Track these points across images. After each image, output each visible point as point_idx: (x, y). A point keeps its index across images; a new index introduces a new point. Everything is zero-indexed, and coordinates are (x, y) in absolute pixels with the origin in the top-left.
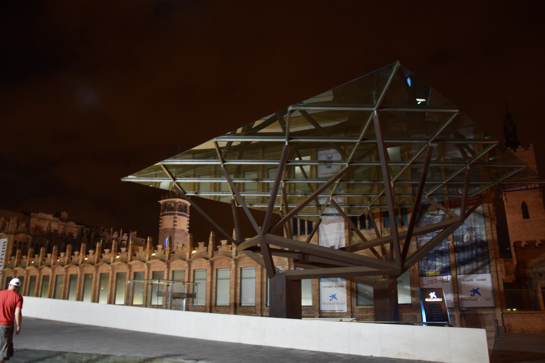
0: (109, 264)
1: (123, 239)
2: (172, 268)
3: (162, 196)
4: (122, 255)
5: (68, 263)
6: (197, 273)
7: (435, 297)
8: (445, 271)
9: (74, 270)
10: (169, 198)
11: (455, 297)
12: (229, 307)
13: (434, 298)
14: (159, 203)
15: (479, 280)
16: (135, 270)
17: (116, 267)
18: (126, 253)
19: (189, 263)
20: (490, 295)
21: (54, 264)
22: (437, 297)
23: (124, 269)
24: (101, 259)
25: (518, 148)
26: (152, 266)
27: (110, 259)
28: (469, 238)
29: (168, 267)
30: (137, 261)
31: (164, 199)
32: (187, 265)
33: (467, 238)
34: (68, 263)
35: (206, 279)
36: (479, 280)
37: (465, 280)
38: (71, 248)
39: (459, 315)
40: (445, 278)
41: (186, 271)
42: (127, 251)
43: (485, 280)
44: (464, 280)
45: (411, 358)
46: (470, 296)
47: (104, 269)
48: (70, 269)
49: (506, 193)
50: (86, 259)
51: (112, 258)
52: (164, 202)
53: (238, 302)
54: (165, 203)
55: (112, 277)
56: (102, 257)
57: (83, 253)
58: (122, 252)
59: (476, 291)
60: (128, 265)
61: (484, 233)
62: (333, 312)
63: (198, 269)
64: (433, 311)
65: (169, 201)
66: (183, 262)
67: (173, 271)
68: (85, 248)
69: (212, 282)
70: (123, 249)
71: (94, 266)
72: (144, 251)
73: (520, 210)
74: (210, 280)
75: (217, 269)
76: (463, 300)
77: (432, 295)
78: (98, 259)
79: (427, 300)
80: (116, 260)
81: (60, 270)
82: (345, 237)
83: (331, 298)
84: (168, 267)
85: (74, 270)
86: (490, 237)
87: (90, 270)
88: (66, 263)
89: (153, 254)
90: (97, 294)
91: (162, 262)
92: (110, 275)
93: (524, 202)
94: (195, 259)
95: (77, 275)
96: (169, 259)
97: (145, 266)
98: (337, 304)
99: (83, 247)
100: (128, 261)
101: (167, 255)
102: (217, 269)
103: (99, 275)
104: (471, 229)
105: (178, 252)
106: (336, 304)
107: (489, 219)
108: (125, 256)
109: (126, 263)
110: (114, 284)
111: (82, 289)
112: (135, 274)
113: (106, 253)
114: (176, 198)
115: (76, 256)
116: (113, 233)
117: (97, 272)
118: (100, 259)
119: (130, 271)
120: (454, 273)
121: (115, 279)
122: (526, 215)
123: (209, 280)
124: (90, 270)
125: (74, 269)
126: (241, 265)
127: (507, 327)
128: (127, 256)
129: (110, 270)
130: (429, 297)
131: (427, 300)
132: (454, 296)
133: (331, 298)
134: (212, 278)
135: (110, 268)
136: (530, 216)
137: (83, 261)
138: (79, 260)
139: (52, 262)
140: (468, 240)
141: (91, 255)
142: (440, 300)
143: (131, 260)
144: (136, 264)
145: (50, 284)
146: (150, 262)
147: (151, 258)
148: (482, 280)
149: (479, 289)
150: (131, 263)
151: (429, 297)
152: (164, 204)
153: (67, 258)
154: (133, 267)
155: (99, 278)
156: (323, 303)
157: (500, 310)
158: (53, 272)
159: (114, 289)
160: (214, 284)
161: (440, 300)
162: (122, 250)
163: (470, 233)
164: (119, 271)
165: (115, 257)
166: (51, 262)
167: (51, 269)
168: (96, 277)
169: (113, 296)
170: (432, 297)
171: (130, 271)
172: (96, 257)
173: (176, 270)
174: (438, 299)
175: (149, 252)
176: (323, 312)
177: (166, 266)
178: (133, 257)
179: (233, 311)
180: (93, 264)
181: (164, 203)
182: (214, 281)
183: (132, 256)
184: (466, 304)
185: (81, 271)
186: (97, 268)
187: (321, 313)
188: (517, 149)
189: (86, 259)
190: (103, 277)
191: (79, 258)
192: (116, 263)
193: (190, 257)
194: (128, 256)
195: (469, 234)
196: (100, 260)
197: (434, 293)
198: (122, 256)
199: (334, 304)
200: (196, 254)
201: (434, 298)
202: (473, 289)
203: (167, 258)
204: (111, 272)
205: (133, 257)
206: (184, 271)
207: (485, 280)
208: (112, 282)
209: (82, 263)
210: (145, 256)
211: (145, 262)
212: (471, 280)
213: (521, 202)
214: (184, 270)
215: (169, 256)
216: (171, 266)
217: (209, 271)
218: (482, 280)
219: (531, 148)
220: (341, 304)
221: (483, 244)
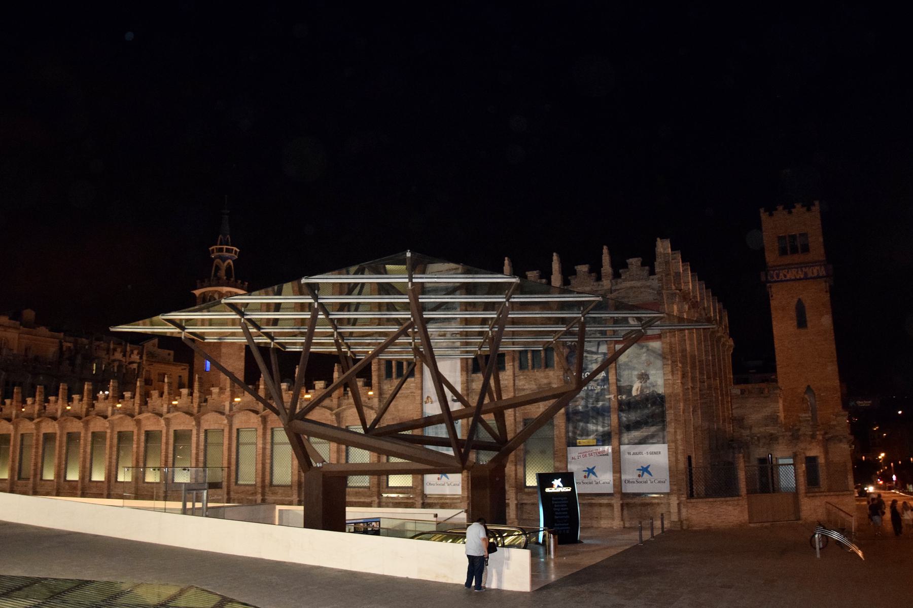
0: (106, 417)
1: (132, 360)
2: (205, 426)
3: (198, 281)
4: (126, 402)
5: (39, 416)
6: (242, 434)
7: (561, 485)
8: (604, 439)
9: (50, 427)
10: (210, 286)
11: (615, 478)
12: (291, 486)
13: (559, 486)
14: (194, 294)
15: (652, 453)
16: (70, 431)
17: (116, 422)
18: (132, 400)
19: (230, 418)
20: (666, 476)
21: (17, 416)
22: (564, 486)
23: (128, 426)
24: (92, 409)
25: (794, 207)
26: (173, 421)
27: (107, 410)
28: (639, 389)
29: (198, 424)
30: (150, 414)
31: (202, 287)
32: (226, 422)
33: (637, 390)
34: (39, 416)
35: (256, 444)
36: (652, 453)
37: (632, 453)
38: (43, 390)
39: (619, 505)
40: (601, 448)
41: (225, 431)
42: (133, 397)
43: (660, 453)
44: (629, 453)
45: (450, 581)
46: (636, 477)
47: (98, 425)
48: (43, 424)
49: (772, 284)
50: (69, 408)
51: (110, 409)
52: (202, 293)
53: (267, 481)
54: (204, 293)
55: (112, 439)
56: (93, 406)
57: (62, 399)
58: (125, 398)
59: (645, 470)
60: (135, 420)
61: (660, 382)
62: (443, 498)
63: (243, 427)
64: (556, 506)
65: (210, 291)
66: (219, 416)
67: (206, 431)
68: (66, 391)
69: (264, 449)
70: (127, 395)
71: (82, 420)
72: (161, 398)
73: (793, 314)
74: (261, 446)
75: (272, 429)
76: (627, 482)
77: (557, 482)
78: (87, 409)
79: (548, 490)
80: (116, 411)
81: (28, 427)
82: (462, 384)
83: (587, 473)
84: (198, 424)
85: (50, 427)
86: (669, 391)
87: (76, 426)
88: (36, 416)
89: (175, 403)
90: (88, 465)
91: (188, 416)
92: (108, 435)
93: (800, 301)
94: (238, 412)
95: (55, 434)
96: (199, 412)
97: (163, 422)
98: (448, 485)
99: (63, 389)
100: (136, 414)
101: (196, 405)
102: (272, 429)
103: (90, 435)
104: (644, 377)
105: (213, 401)
106: (446, 484)
107: (670, 362)
108: (130, 405)
109: (132, 416)
110: (115, 449)
111: (64, 456)
112: (148, 433)
113: (100, 400)
114: (222, 285)
115: (51, 404)
116: (115, 350)
117: (87, 429)
118: (90, 409)
119: (139, 429)
120: (615, 441)
121: (115, 441)
122: (802, 322)
123: (260, 445)
124: (76, 426)
125: (50, 424)
126: (237, 424)
127: (685, 522)
128: (134, 405)
129: (107, 428)
130: (551, 486)
131: (548, 490)
132: (613, 476)
133: (586, 474)
134: (264, 443)
135: (107, 425)
136: (809, 325)
137: (65, 412)
138: (57, 410)
139: (14, 412)
140: (639, 393)
141: (76, 402)
142: (568, 489)
143: (140, 413)
144: (148, 418)
145: (11, 448)
146: (169, 416)
147: (172, 409)
148: (656, 453)
149: (650, 467)
150: (141, 417)
151: (551, 486)
152: (202, 296)
153: (37, 407)
154: (143, 422)
155: (90, 439)
156: (428, 484)
157: (676, 498)
158: (16, 429)
159: (114, 457)
160: (268, 452)
161: (568, 489)
162: (126, 396)
163: (641, 382)
164: (122, 429)
165: (114, 406)
166: (12, 413)
167: (13, 424)
168: (86, 439)
169: (114, 469)
170: (556, 486)
171: (139, 429)
172: (85, 407)
173: (210, 429)
174: (565, 488)
175: (167, 399)
176: (428, 496)
177: (194, 423)
178: (144, 408)
179: (297, 493)
180: (79, 418)
181: (200, 294)
182: (268, 446)
183: (140, 405)
184: (629, 489)
185: (62, 428)
186: (87, 424)
187: (425, 499)
188: (793, 210)
189: (69, 408)
190: (98, 437)
191: (57, 406)
192: (117, 417)
193: (231, 410)
194: (135, 405)
195: (641, 384)
196: (91, 411)
197: (560, 479)
198: (126, 404)
199: (444, 485)
200: (241, 404)
201: (559, 486)
202: (642, 467)
203: (195, 410)
204: (109, 431)
205: (142, 407)
206: (223, 430)
207: (660, 453)
208: (111, 448)
209: (62, 415)
210: (162, 406)
211: (161, 415)
212: (640, 453)
213: (796, 300)
214: (222, 428)
215: (199, 406)
216: (202, 421)
217: (260, 432)
218: (656, 453)
219: (816, 208)
220: (454, 485)
221: (658, 400)
